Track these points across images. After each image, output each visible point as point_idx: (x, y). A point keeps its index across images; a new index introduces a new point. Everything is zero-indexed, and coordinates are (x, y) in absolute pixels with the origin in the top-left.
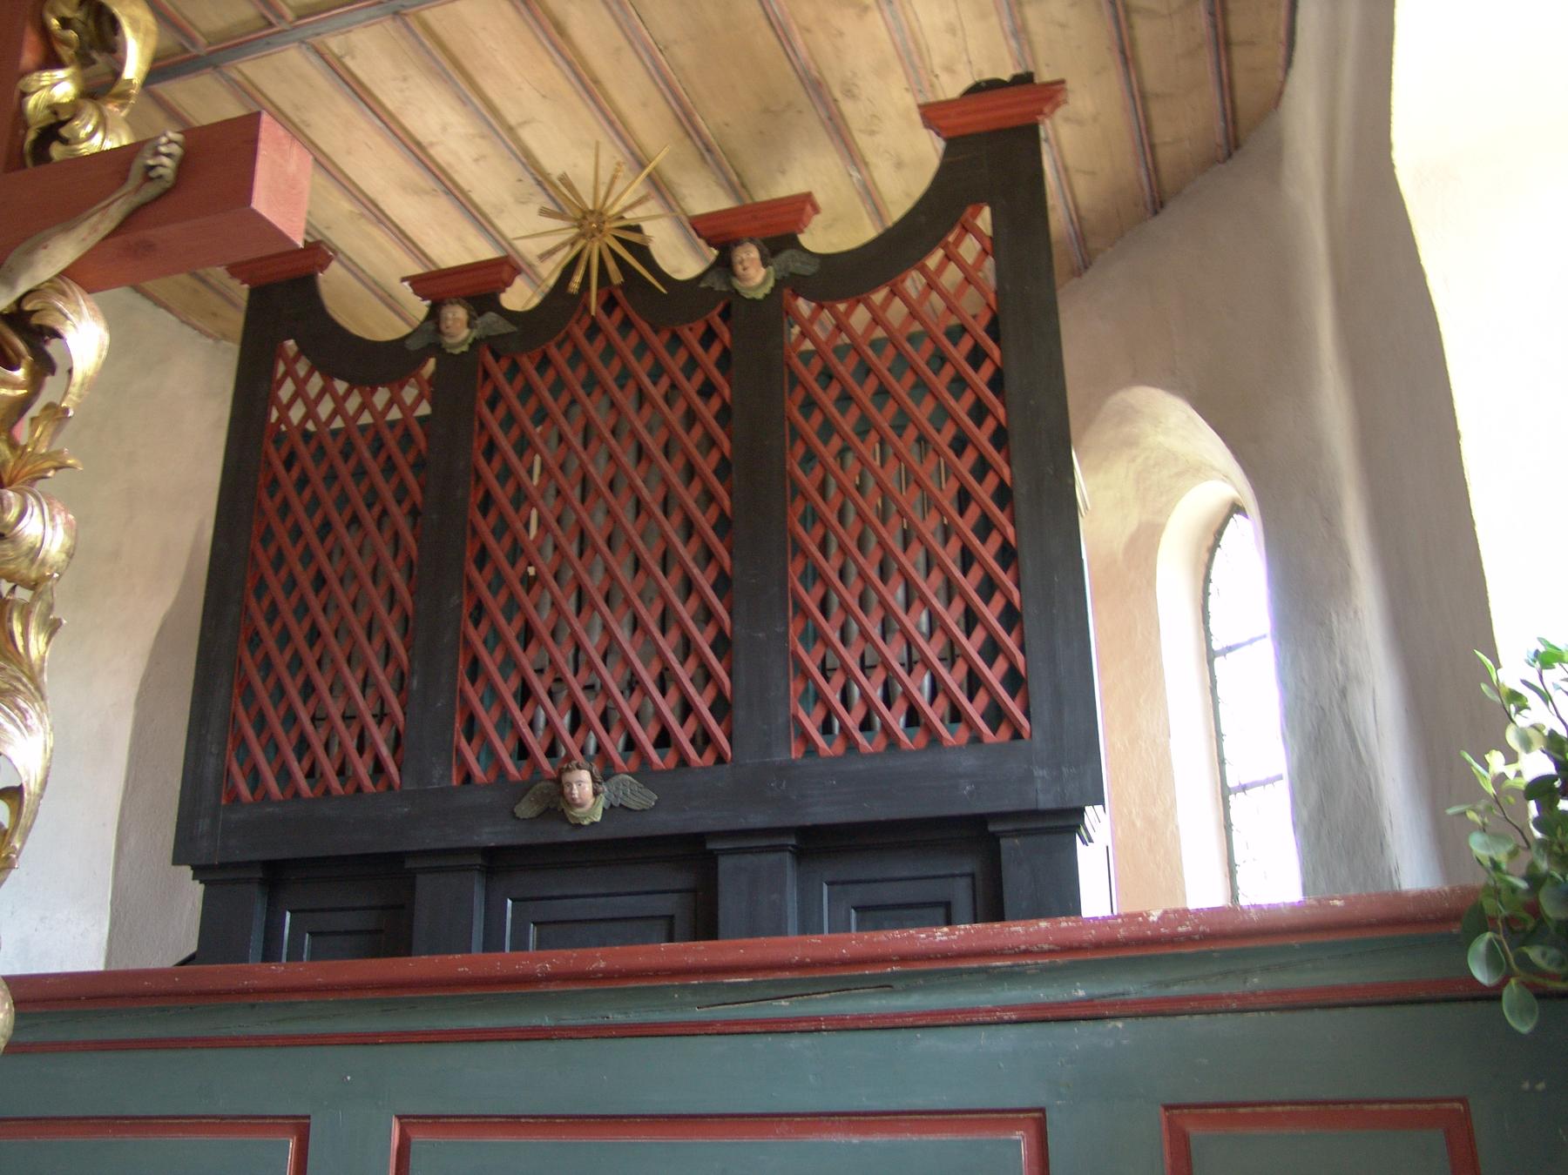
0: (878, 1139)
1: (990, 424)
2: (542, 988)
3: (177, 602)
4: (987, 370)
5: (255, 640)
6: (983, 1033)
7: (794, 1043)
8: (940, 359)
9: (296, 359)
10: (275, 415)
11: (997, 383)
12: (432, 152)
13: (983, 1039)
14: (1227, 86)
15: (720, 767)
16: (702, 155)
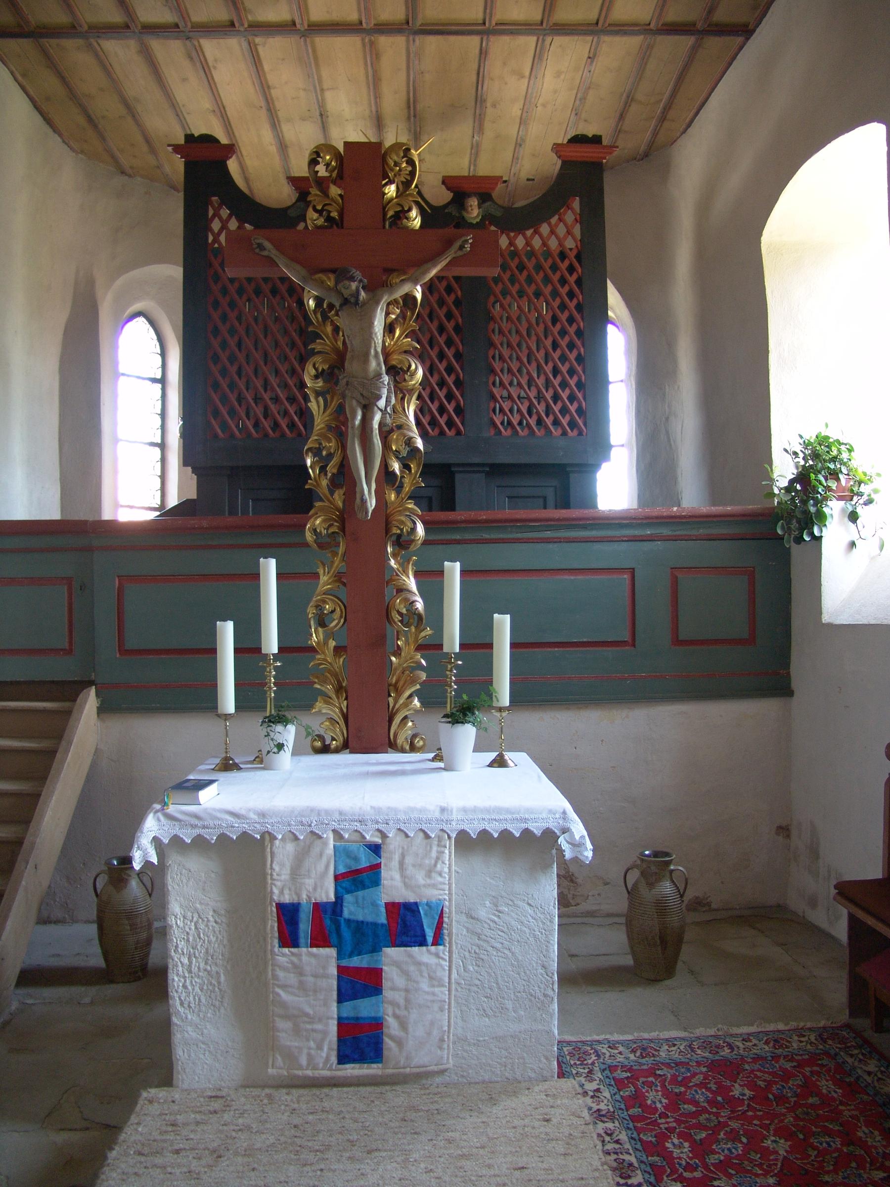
1: (575, 301)
2: (459, 525)
4: (575, 276)
5: (216, 359)
6: (616, 544)
7: (551, 546)
8: (554, 268)
9: (220, 207)
11: (579, 282)
12: (272, 91)
13: (615, 546)
14: (655, 134)
15: (458, 437)
16: (409, 118)
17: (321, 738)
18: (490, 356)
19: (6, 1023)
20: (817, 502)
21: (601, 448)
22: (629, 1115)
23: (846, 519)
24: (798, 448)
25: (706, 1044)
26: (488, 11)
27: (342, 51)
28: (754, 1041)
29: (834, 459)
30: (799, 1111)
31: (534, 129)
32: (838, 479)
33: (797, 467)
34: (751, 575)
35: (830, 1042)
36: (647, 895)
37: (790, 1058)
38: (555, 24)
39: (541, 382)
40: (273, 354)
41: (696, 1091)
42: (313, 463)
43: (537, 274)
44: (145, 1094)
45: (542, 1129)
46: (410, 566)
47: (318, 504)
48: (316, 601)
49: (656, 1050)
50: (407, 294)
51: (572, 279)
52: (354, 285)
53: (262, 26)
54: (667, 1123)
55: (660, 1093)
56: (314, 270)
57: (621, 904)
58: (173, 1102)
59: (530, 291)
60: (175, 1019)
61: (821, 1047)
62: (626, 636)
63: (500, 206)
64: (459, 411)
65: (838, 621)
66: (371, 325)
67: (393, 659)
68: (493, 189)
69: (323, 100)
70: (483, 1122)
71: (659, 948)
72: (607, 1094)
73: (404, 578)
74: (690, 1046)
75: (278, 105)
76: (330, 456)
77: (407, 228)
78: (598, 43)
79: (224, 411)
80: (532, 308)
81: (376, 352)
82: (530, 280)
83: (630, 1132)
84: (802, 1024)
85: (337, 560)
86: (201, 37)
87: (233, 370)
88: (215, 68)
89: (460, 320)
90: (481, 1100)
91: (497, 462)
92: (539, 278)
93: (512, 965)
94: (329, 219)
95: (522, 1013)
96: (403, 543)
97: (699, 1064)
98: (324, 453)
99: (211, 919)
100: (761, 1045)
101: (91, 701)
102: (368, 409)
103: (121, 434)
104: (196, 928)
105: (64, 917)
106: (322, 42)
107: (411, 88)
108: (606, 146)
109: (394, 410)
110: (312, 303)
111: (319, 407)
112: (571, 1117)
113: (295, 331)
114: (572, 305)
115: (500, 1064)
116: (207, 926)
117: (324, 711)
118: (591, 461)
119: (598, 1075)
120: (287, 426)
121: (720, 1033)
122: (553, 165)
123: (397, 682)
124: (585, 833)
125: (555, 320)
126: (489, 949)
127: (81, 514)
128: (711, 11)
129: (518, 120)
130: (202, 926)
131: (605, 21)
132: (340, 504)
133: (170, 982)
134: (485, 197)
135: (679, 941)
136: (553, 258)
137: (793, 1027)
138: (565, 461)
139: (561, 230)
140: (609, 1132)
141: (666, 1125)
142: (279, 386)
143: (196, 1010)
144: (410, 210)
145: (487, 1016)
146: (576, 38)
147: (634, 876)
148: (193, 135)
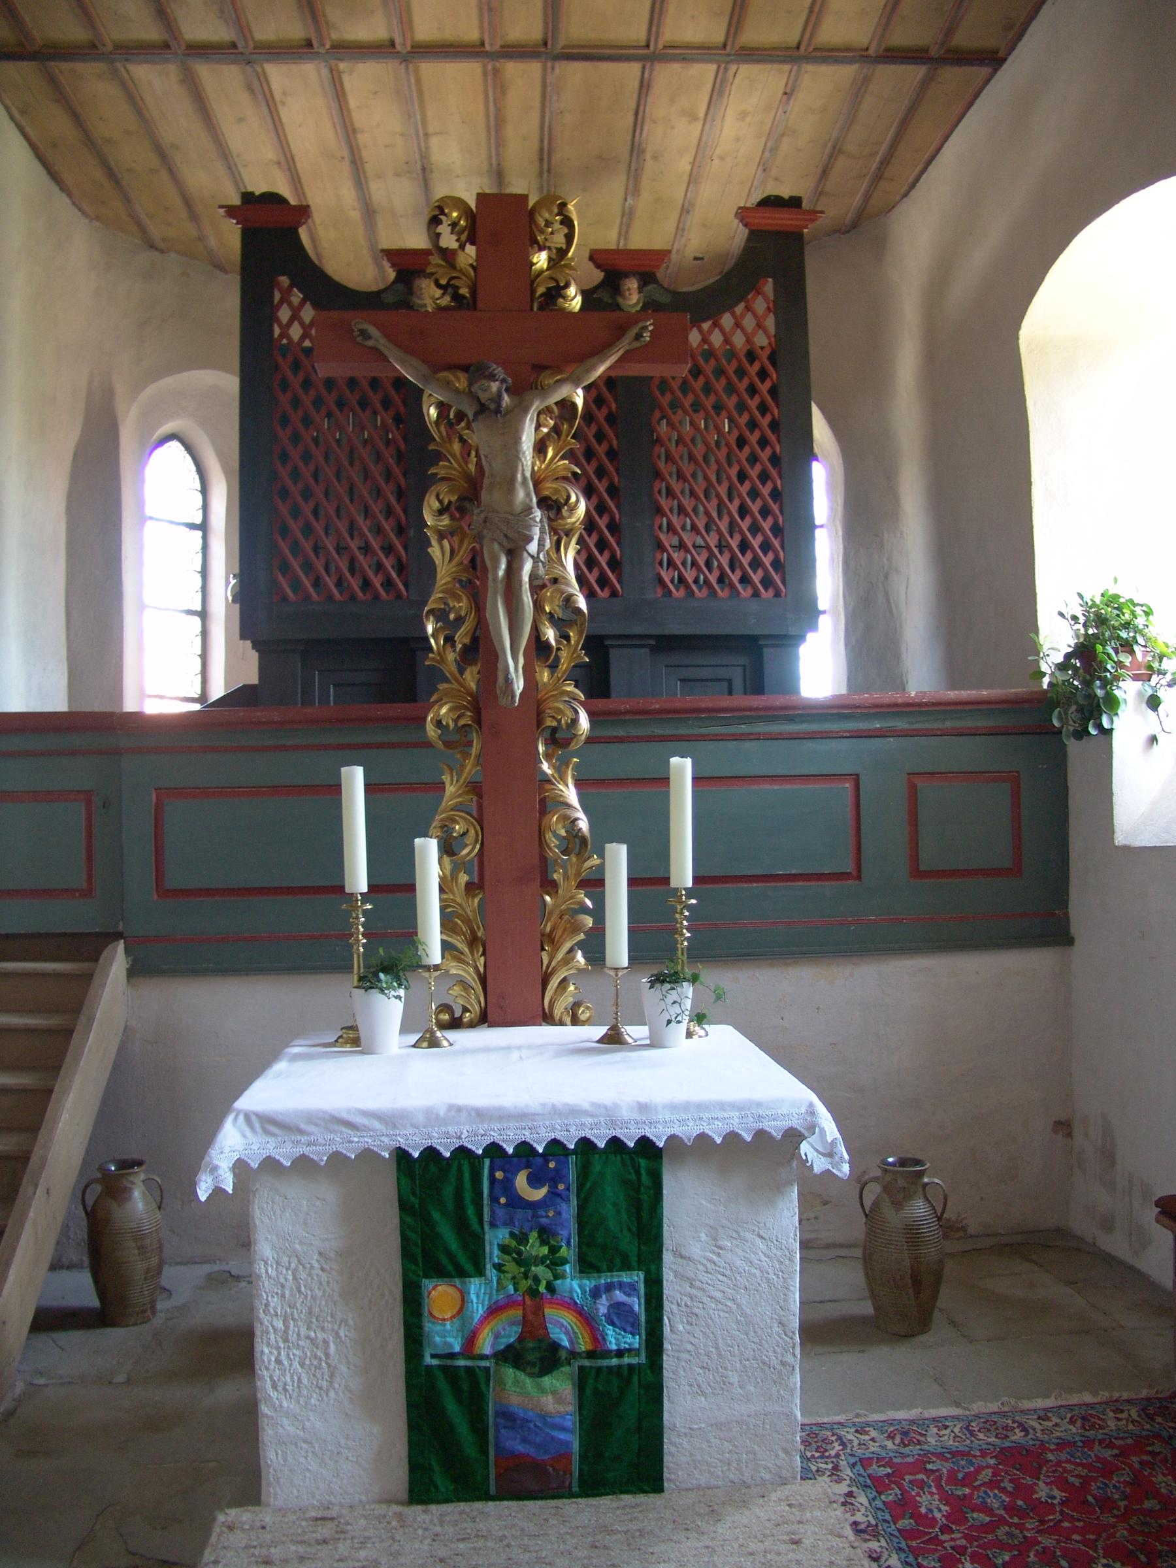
0: (787, 787)
2: (622, 717)
3: (83, 431)
5: (284, 493)
7: (747, 745)
8: (741, 373)
9: (289, 290)
10: (277, 331)
11: (773, 391)
12: (359, 136)
13: (834, 744)
14: (868, 196)
16: (541, 174)
17: (445, 1007)
18: (656, 490)
19: (10, 1414)
20: (1105, 683)
21: (806, 613)
22: (899, 1530)
23: (1144, 706)
24: (1079, 612)
25: (989, 1424)
26: (654, 29)
27: (456, 81)
28: (1055, 1420)
29: (1126, 626)
30: (1133, 1521)
31: (707, 191)
32: (1132, 652)
33: (1078, 637)
34: (1015, 780)
35: (1159, 1419)
36: (893, 1218)
37: (1107, 1443)
38: (742, 48)
39: (723, 525)
40: (363, 489)
41: (985, 1492)
42: (435, 631)
43: (718, 381)
44: (221, 1518)
45: (791, 1556)
46: (570, 772)
47: (441, 686)
48: (442, 820)
49: (921, 1434)
50: (563, 400)
51: (764, 388)
52: (495, 386)
53: (349, 47)
54: (952, 1539)
55: (936, 1497)
56: (436, 367)
57: (857, 1229)
58: (263, 1528)
59: (709, 403)
60: (264, 1408)
61: (1148, 1427)
62: (849, 867)
63: (667, 290)
64: (614, 564)
65: (1138, 843)
66: (517, 440)
67: (548, 898)
68: (658, 267)
69: (427, 148)
70: (707, 1547)
71: (911, 1291)
72: (863, 1499)
73: (561, 787)
74: (967, 1428)
75: (365, 154)
76: (460, 620)
77: (562, 310)
78: (798, 72)
79: (295, 565)
80: (711, 427)
81: (524, 478)
82: (708, 389)
83: (903, 1556)
84: (1116, 1395)
85: (469, 764)
86: (268, 61)
87: (308, 508)
88: (283, 103)
89: (615, 442)
90: (700, 1515)
91: (667, 632)
92: (720, 385)
93: (738, 1322)
94: (456, 297)
95: (752, 1389)
96: (559, 739)
97: (984, 1454)
98: (452, 616)
99: (316, 1265)
100: (1065, 1425)
101: (118, 961)
102: (514, 554)
103: (147, 600)
104: (295, 1278)
105: (81, 1260)
106: (429, 69)
107: (546, 133)
108: (808, 211)
109: (550, 559)
110: (433, 412)
111: (443, 555)
112: (829, 1537)
113: (392, 456)
114: (765, 422)
115: (721, 1461)
116: (310, 1275)
117: (453, 971)
118: (792, 631)
119: (847, 1472)
120: (382, 585)
121: (1006, 1409)
122: (736, 236)
123: (551, 932)
124: (838, 1136)
125: (741, 442)
126: (706, 1299)
127: (96, 706)
128: (950, 31)
129: (686, 178)
130: (303, 1276)
131: (809, 45)
132: (473, 686)
133: (257, 1355)
134: (647, 279)
135: (938, 1279)
136: (739, 361)
137: (1104, 1399)
138: (757, 631)
139: (749, 322)
140: (874, 1555)
141: (953, 1544)
142: (370, 531)
143: (295, 1394)
144: (567, 286)
145: (703, 1393)
146: (769, 66)
147: (873, 1192)
148: (252, 194)
